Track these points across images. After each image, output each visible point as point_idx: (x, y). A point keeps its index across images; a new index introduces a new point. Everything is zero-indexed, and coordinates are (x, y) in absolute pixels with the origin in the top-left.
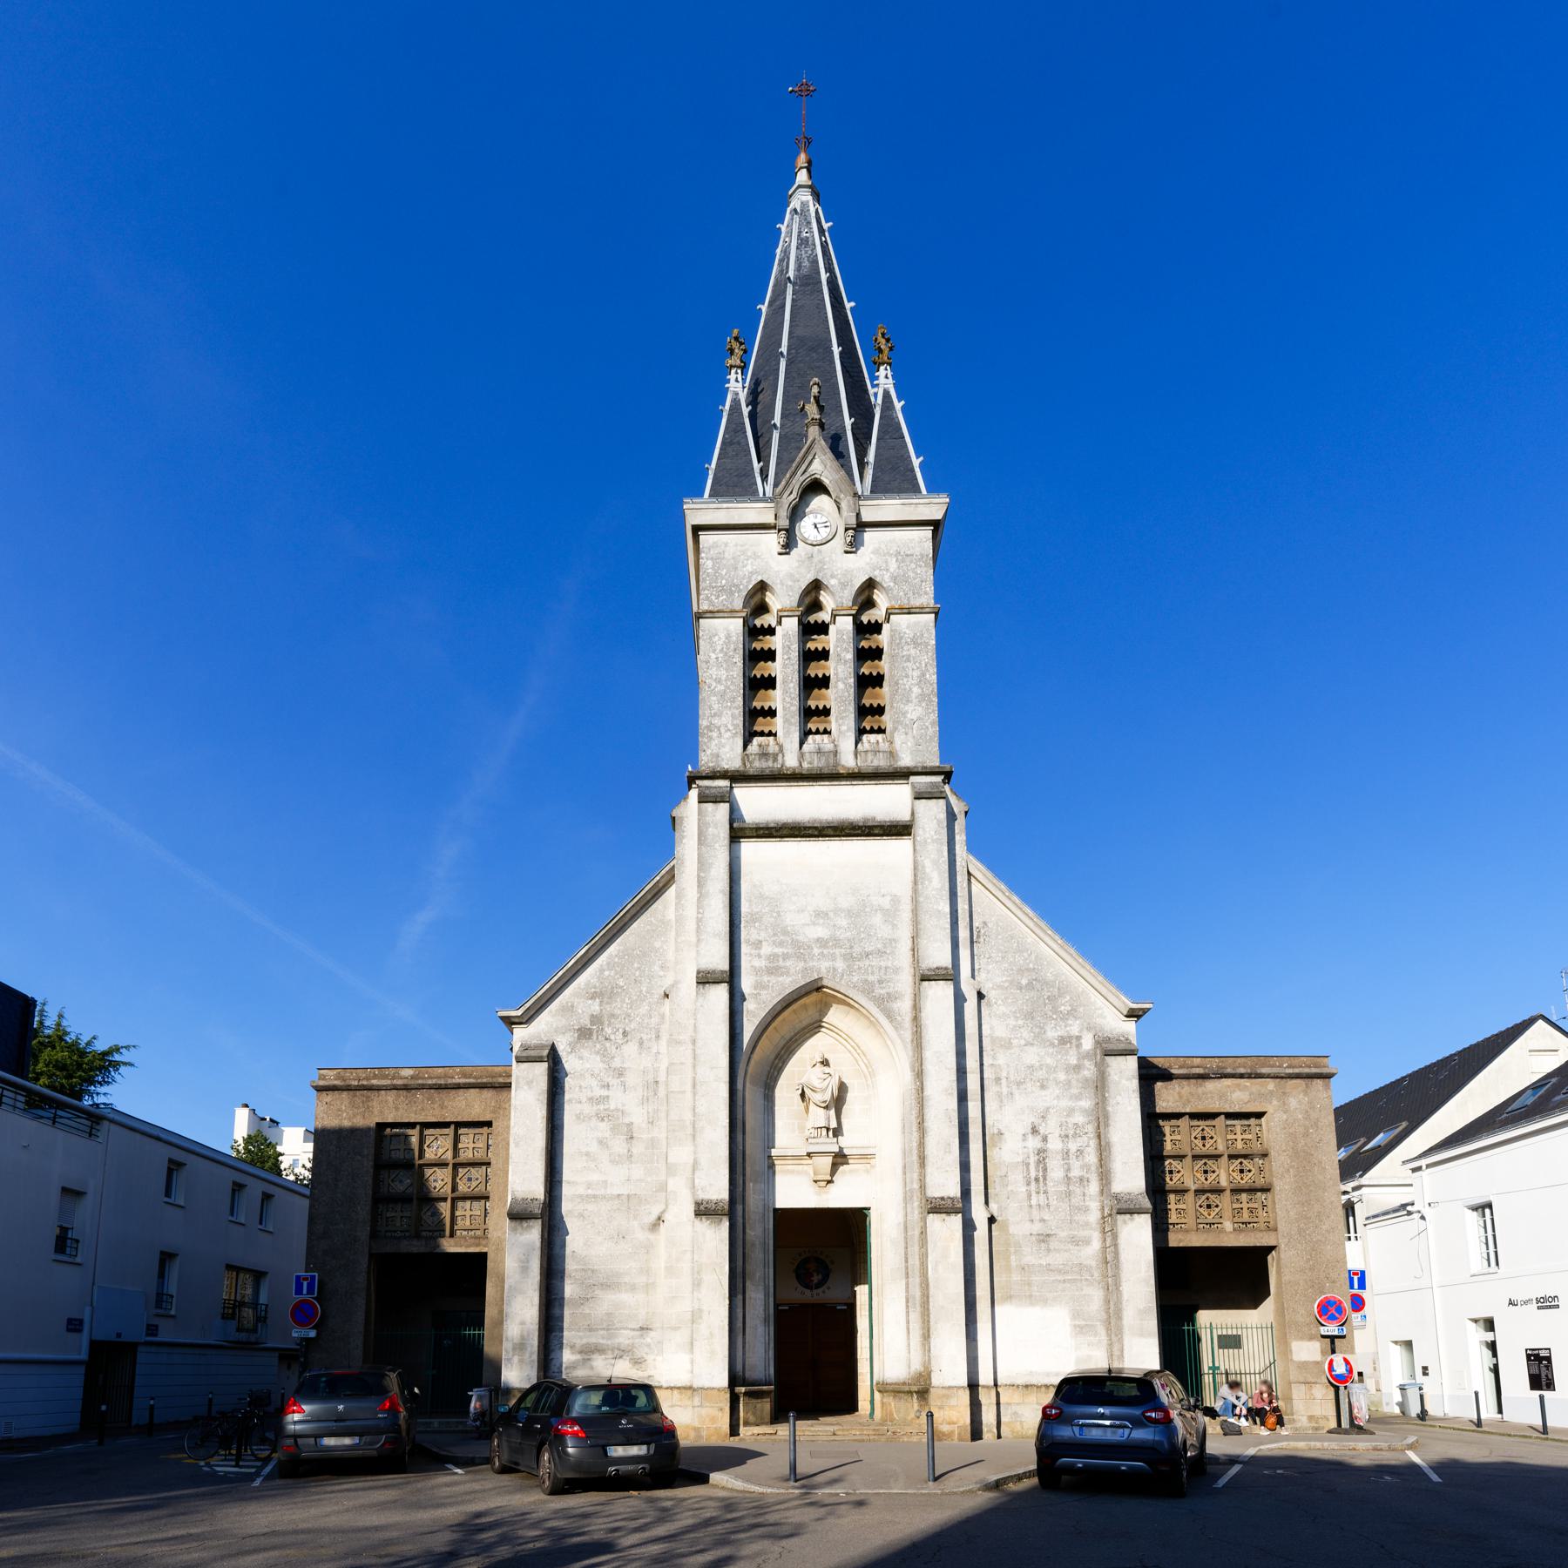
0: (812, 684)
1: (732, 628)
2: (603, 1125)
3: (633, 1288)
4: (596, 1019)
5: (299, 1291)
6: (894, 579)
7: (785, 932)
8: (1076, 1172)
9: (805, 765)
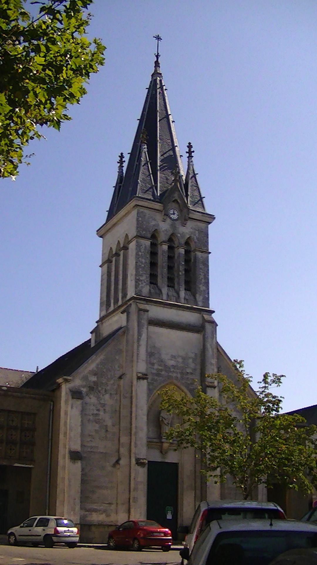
0: (170, 268)
1: (147, 244)
2: (97, 425)
6: (197, 239)
7: (162, 361)
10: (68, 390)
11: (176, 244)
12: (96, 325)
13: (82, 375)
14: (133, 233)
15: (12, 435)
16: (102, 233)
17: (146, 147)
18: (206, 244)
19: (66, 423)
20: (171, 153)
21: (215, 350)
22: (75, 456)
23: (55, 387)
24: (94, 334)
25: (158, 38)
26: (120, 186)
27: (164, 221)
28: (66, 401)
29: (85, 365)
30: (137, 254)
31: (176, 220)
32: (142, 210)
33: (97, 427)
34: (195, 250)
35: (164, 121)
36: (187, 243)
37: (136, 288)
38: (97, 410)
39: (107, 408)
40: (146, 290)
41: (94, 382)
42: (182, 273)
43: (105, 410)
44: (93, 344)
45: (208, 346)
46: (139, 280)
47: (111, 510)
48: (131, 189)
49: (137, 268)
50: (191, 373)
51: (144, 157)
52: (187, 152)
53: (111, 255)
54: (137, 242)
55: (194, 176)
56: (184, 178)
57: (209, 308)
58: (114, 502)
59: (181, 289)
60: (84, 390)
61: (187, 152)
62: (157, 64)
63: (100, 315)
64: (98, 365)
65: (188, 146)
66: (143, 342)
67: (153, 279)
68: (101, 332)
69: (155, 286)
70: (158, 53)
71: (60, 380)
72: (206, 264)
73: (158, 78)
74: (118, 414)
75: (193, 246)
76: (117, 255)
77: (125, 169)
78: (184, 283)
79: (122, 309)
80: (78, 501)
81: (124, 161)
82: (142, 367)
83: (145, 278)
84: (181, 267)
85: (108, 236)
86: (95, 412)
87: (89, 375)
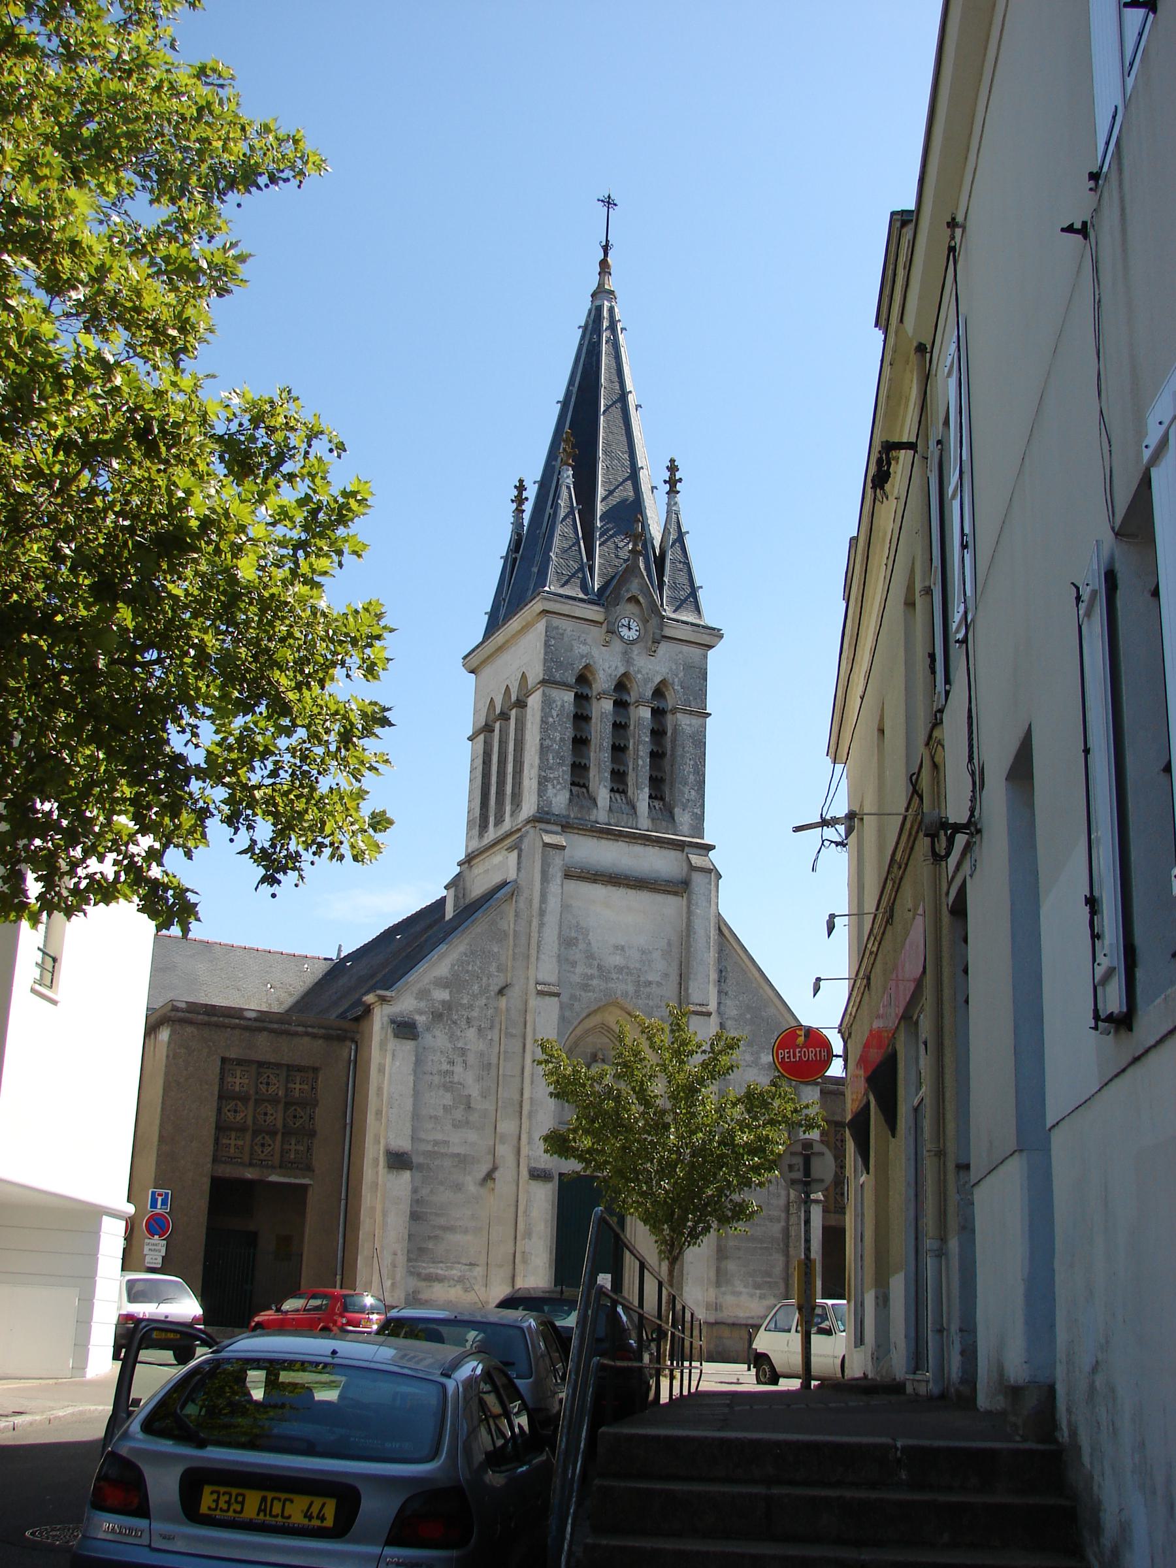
0: (618, 750)
1: (566, 698)
2: (448, 1095)
3: (466, 1231)
4: (448, 1006)
5: (154, 1205)
8: (290, 771)
9: (849, 1374)
10: (386, 1019)
11: (632, 698)
12: (458, 869)
13: (415, 989)
14: (536, 673)
15: (266, 1114)
16: (474, 663)
17: (571, 472)
18: (701, 694)
19: (380, 1089)
20: (628, 492)
21: (713, 933)
22: (398, 1161)
23: (359, 1011)
24: (452, 890)
25: (609, 202)
26: (515, 560)
27: (606, 644)
28: (383, 1044)
29: (421, 968)
30: (544, 721)
31: (633, 642)
32: (556, 621)
33: (448, 1099)
34: (674, 711)
35: (616, 411)
36: (658, 693)
37: (540, 796)
38: (449, 1063)
39: (472, 1058)
40: (560, 799)
41: (443, 1002)
42: (644, 762)
43: (465, 1062)
44: (449, 913)
45: (698, 925)
46: (546, 779)
47: (475, 1278)
48: (535, 570)
49: (543, 750)
50: (659, 984)
51: (566, 497)
52: (665, 482)
53: (492, 717)
54: (544, 694)
55: (680, 538)
56: (657, 544)
57: (703, 838)
58: (482, 1260)
59: (641, 797)
60: (421, 1020)
61: (665, 482)
62: (604, 265)
63: (467, 847)
64: (453, 965)
65: (516, 487)
66: (552, 919)
67: (579, 773)
68: (468, 885)
69: (584, 790)
70: (607, 241)
71: (370, 998)
72: (700, 743)
73: (606, 303)
74: (493, 1072)
75: (671, 701)
76: (504, 716)
77: (527, 517)
78: (647, 782)
79: (508, 842)
80: (401, 1259)
81: (527, 499)
82: (547, 970)
83: (563, 773)
84: (641, 747)
85: (487, 671)
86: (445, 1067)
87: (432, 987)
